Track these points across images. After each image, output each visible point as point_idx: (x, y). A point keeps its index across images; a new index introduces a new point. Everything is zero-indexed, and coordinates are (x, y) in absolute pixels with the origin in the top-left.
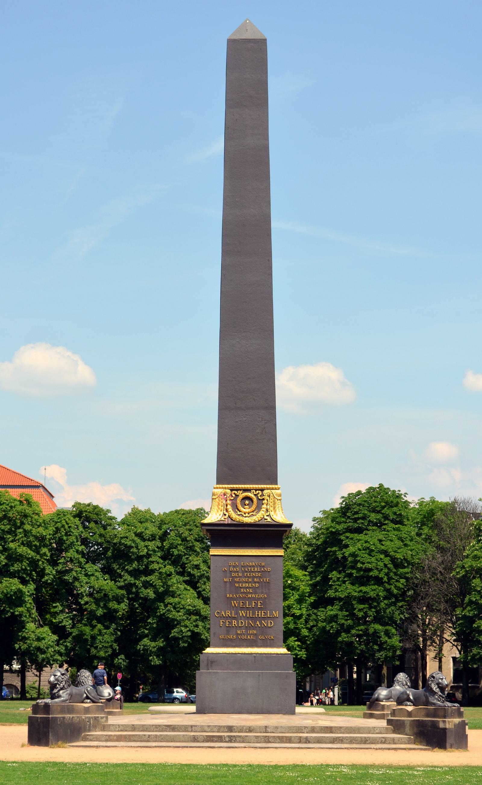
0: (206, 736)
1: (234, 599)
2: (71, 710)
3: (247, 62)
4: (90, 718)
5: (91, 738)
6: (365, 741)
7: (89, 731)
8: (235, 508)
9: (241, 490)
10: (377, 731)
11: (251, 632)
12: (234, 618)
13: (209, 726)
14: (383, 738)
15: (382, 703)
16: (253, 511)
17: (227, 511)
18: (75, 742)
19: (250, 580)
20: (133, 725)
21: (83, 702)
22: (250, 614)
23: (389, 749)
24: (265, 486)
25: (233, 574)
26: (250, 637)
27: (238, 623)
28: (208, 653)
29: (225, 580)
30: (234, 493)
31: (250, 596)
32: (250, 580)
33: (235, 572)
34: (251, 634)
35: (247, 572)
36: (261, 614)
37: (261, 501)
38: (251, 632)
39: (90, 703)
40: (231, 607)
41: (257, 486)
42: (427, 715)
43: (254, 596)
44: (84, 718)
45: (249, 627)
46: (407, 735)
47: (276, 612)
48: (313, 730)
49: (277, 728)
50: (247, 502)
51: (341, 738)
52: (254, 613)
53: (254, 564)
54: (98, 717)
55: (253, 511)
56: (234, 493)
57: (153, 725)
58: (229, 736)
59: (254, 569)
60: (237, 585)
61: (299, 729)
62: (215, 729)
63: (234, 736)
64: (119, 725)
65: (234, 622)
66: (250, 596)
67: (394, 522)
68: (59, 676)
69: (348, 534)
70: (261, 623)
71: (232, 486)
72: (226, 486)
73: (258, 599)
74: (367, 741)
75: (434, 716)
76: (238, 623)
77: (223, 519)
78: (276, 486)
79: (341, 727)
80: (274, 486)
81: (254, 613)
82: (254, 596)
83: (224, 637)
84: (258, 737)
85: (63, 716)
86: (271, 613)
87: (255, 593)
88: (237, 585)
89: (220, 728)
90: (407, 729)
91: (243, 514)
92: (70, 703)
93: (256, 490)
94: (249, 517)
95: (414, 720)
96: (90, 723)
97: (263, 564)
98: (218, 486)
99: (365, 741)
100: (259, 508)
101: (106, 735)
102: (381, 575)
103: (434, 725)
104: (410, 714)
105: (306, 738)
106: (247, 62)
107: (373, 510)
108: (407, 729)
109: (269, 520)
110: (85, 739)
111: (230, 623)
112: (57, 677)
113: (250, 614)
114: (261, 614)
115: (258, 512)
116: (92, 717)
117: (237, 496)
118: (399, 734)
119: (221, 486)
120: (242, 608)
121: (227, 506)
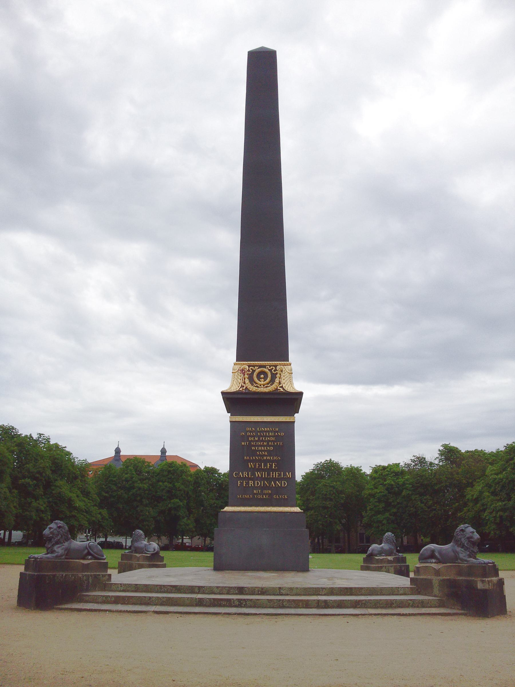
0: (214, 599)
1: (250, 461)
2: (65, 566)
3: (262, 67)
4: (88, 576)
5: (87, 598)
6: (389, 604)
7: (87, 590)
8: (252, 381)
9: (257, 366)
10: (401, 592)
11: (266, 492)
12: (251, 479)
13: (218, 587)
14: (411, 600)
15: (377, 558)
16: (268, 384)
17: (244, 383)
18: (65, 604)
19: (265, 444)
20: (136, 585)
21: (84, 558)
22: (265, 475)
23: (421, 614)
24: (278, 362)
25: (250, 439)
26: (266, 496)
27: (254, 483)
28: (225, 512)
29: (243, 444)
30: (252, 369)
31: (265, 458)
32: (265, 444)
33: (252, 436)
34: (266, 494)
35: (262, 436)
36: (276, 475)
37: (274, 376)
38: (266, 492)
39: (91, 559)
40: (248, 469)
41: (271, 363)
42: (460, 574)
43: (269, 458)
44: (80, 576)
45: (265, 488)
46: (435, 596)
47: (289, 474)
48: (332, 591)
49: (291, 589)
50: (262, 376)
51: (364, 602)
52: (269, 474)
53: (268, 429)
54: (99, 575)
55: (268, 384)
56: (252, 369)
57: (157, 585)
58: (238, 599)
59: (269, 434)
60: (253, 448)
61: (317, 591)
62: (225, 591)
63: (244, 600)
64: (121, 584)
65: (251, 483)
66: (265, 458)
67: (337, 474)
68: (55, 529)
69: (317, 480)
70: (275, 483)
71: (249, 362)
72: (244, 363)
73: (273, 461)
74: (393, 604)
75: (469, 575)
76: (254, 483)
77: (241, 389)
78: (288, 363)
79: (361, 588)
80: (285, 362)
81: (269, 474)
82: (269, 458)
83: (242, 496)
84: (271, 600)
85: (54, 573)
86: (285, 474)
87: (270, 456)
88: (253, 448)
89: (229, 590)
90: (436, 590)
91: (259, 385)
92: (66, 559)
93: (270, 366)
94: (263, 387)
95: (444, 580)
96: (89, 582)
97: (277, 429)
98: (237, 362)
99: (389, 604)
100: (272, 381)
101: (103, 596)
102: (332, 497)
103: (471, 586)
104: (437, 573)
105: (325, 601)
106: (262, 67)
107: (329, 470)
108: (436, 590)
109: (282, 390)
110: (81, 600)
111: (248, 483)
112: (52, 530)
113: (265, 475)
114: (276, 475)
115: (272, 385)
116: (91, 575)
117: (254, 371)
118: (425, 595)
119: (239, 363)
120: (258, 470)
121: (245, 379)
